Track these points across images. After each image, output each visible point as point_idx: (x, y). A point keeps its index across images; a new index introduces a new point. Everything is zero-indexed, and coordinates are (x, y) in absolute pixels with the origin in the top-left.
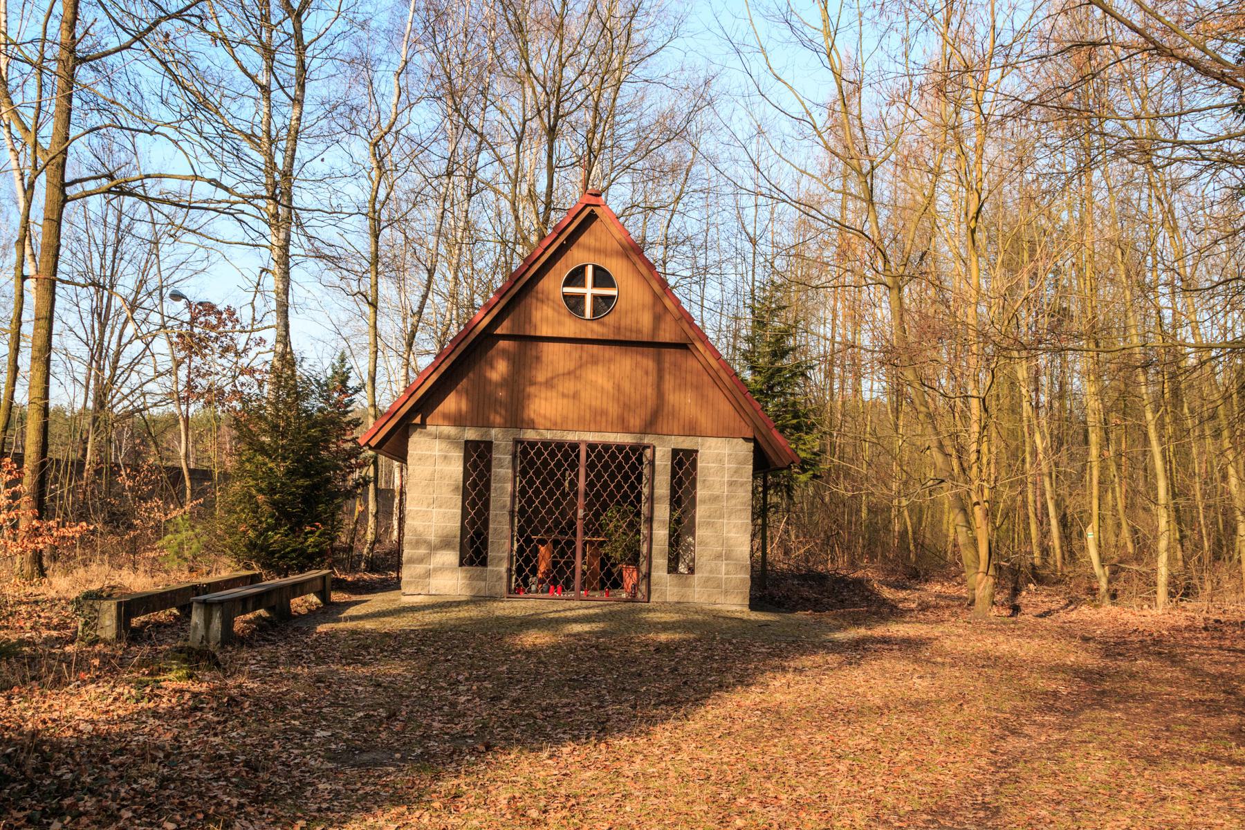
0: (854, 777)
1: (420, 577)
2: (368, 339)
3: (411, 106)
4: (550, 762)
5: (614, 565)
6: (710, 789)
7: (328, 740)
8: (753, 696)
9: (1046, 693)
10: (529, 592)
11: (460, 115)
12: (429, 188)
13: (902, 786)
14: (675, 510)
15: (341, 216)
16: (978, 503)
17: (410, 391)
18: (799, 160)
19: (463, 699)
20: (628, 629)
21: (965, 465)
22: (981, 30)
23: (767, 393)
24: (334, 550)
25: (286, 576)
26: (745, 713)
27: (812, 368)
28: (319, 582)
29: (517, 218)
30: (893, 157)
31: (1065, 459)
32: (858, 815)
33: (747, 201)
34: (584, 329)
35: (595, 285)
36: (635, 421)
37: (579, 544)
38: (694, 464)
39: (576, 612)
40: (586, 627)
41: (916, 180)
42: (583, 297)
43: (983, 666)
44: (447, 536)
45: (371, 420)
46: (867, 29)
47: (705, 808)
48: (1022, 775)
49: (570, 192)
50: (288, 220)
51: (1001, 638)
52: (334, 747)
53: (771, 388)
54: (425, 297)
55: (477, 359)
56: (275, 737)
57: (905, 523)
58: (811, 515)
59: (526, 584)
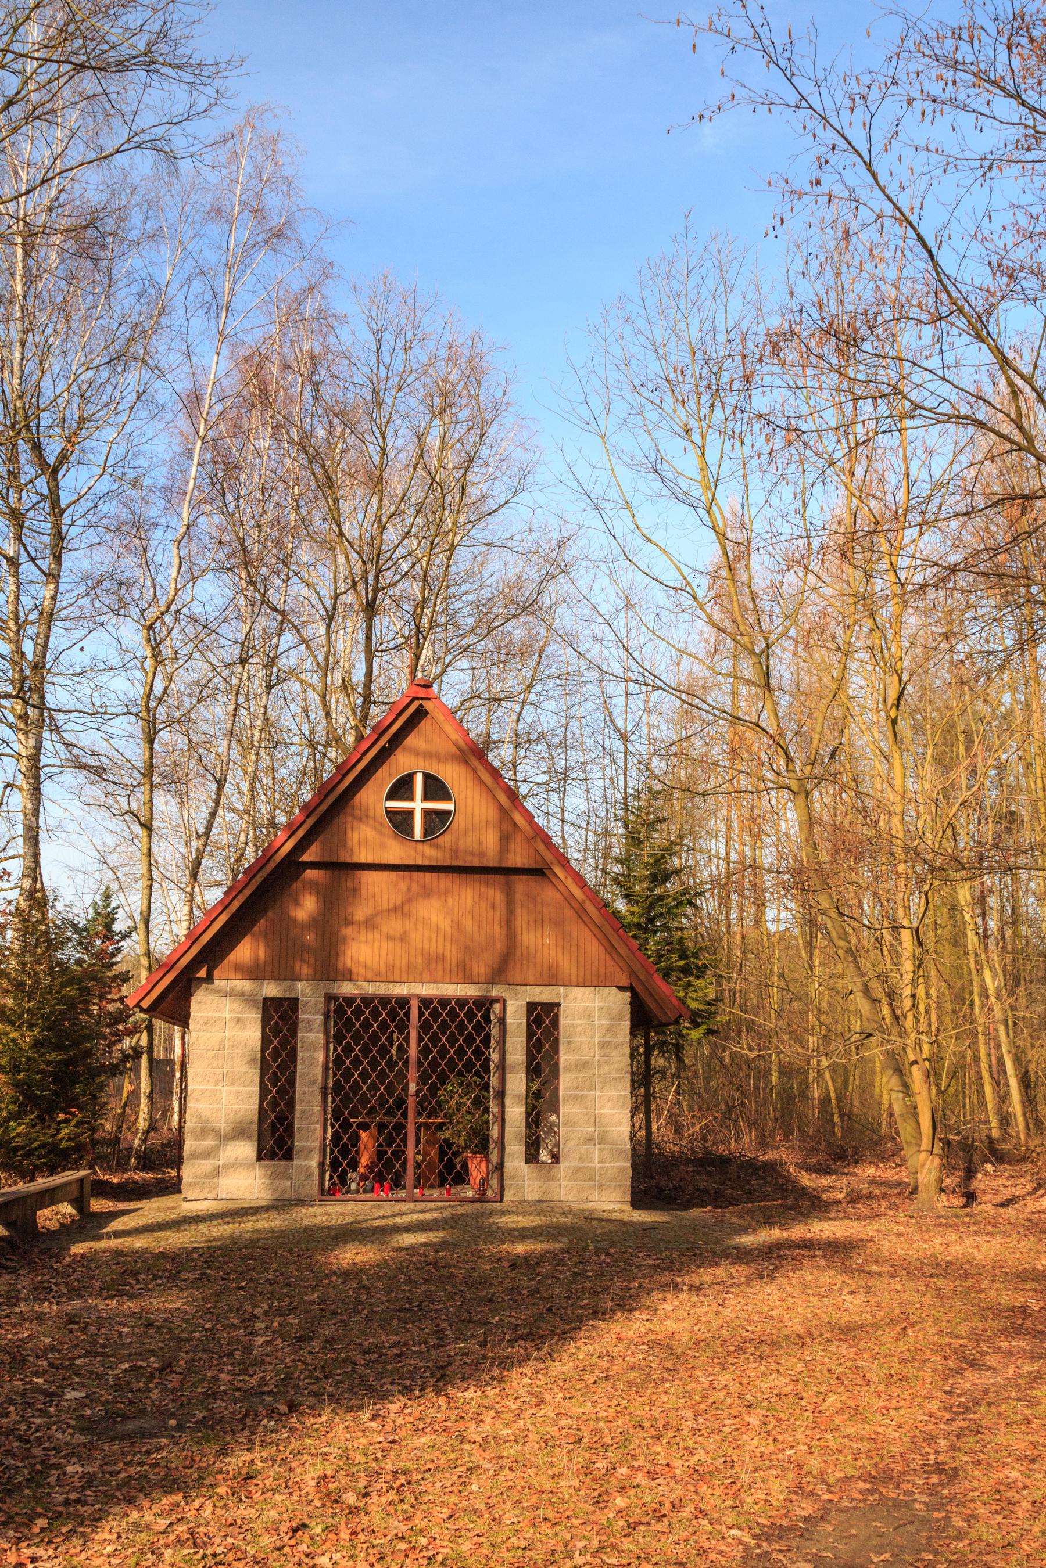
0: (768, 1433)
1: (206, 1176)
2: (140, 868)
3: (194, 579)
4: (373, 1424)
5: (456, 1154)
6: (582, 1456)
7: (81, 1403)
8: (637, 1325)
9: (1012, 1309)
10: (348, 1192)
11: (256, 590)
12: (217, 680)
13: (831, 1443)
14: (533, 1081)
15: (106, 717)
16: (915, 1062)
17: (193, 937)
18: (676, 636)
19: (260, 1340)
20: (475, 1238)
21: (899, 1012)
22: (892, 479)
23: (646, 927)
24: (94, 1143)
25: (32, 1180)
26: (627, 1348)
27: (701, 894)
28: (74, 1187)
29: (328, 715)
30: (792, 633)
31: (1023, 1002)
32: (775, 1486)
33: (615, 689)
34: (412, 853)
35: (426, 797)
36: (480, 969)
37: (411, 1128)
38: (555, 1022)
39: (407, 1218)
40: (422, 1238)
41: (822, 660)
42: (410, 813)
43: (931, 1276)
44: (240, 1122)
45: (144, 974)
46: (754, 480)
47: (576, 1483)
48: (984, 1423)
49: (394, 680)
50: (40, 724)
51: (953, 1237)
52: (89, 1412)
53: (651, 921)
54: (213, 814)
55: (282, 893)
56: (11, 1402)
57: (827, 1088)
58: (708, 1079)
59: (343, 1181)
